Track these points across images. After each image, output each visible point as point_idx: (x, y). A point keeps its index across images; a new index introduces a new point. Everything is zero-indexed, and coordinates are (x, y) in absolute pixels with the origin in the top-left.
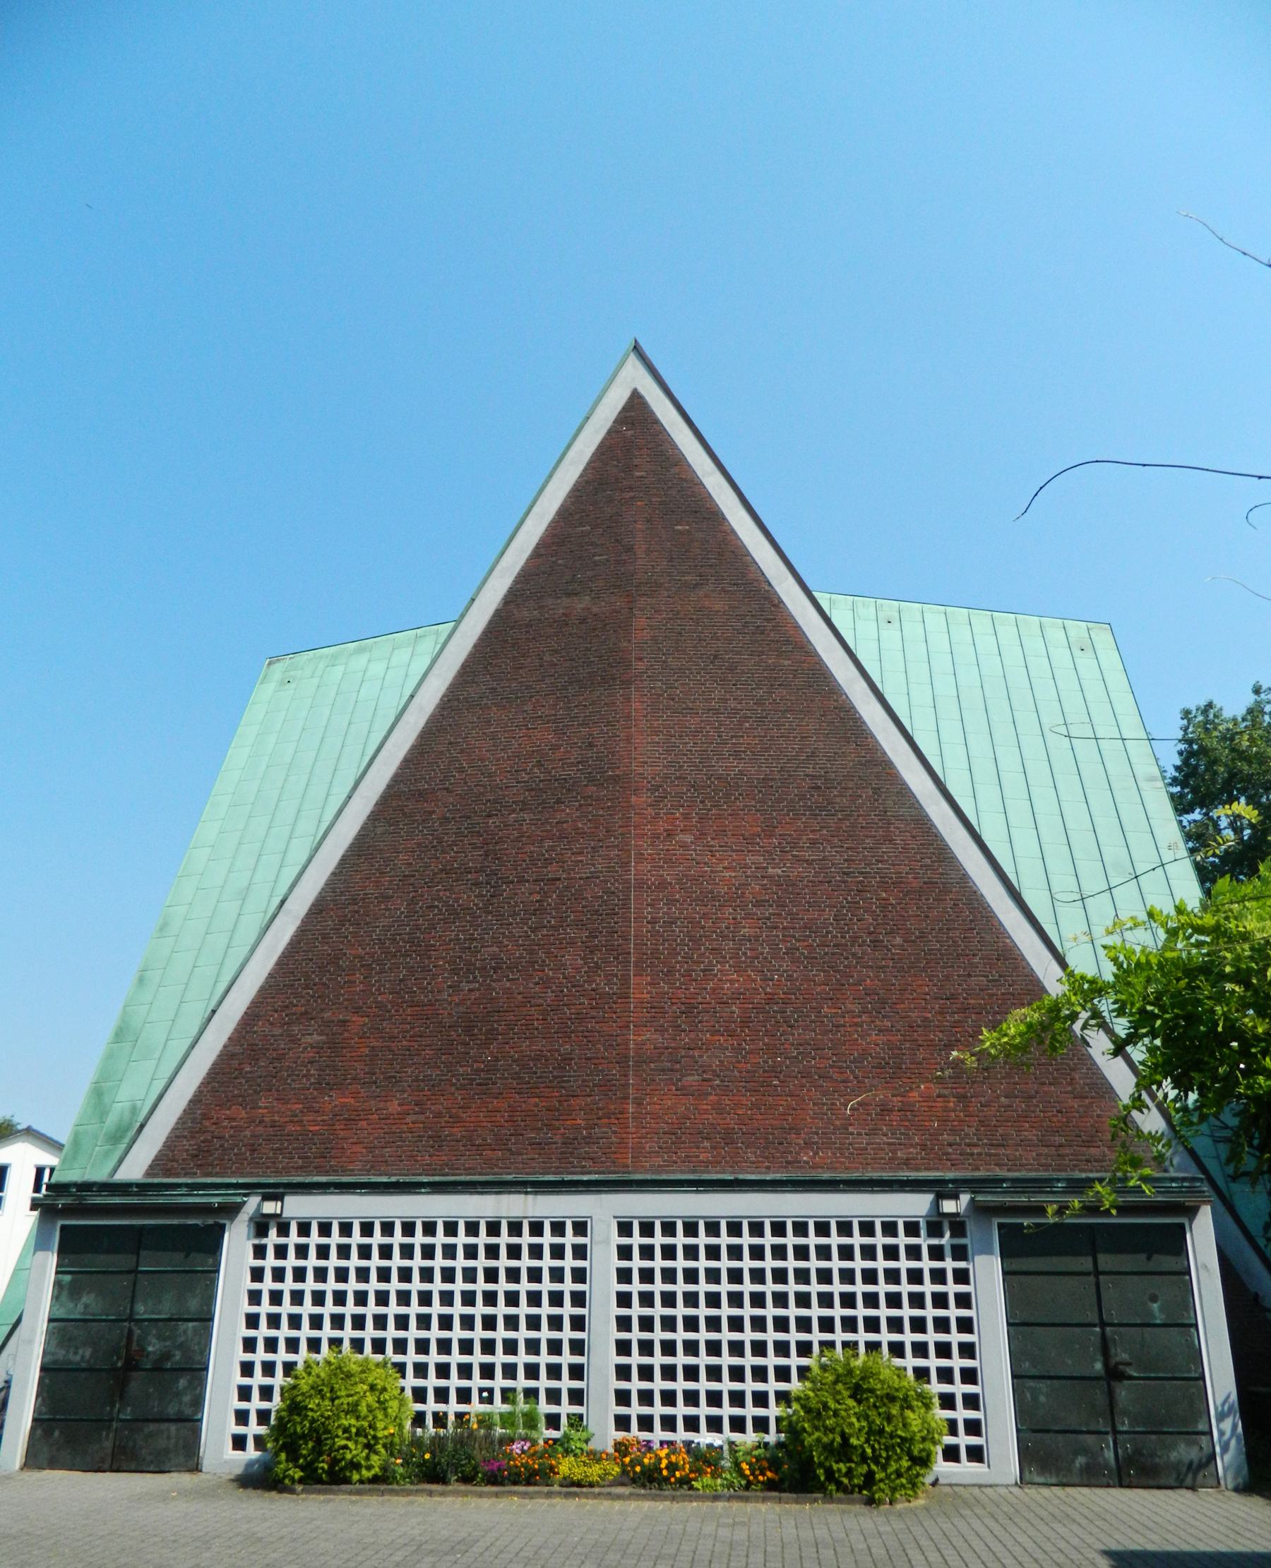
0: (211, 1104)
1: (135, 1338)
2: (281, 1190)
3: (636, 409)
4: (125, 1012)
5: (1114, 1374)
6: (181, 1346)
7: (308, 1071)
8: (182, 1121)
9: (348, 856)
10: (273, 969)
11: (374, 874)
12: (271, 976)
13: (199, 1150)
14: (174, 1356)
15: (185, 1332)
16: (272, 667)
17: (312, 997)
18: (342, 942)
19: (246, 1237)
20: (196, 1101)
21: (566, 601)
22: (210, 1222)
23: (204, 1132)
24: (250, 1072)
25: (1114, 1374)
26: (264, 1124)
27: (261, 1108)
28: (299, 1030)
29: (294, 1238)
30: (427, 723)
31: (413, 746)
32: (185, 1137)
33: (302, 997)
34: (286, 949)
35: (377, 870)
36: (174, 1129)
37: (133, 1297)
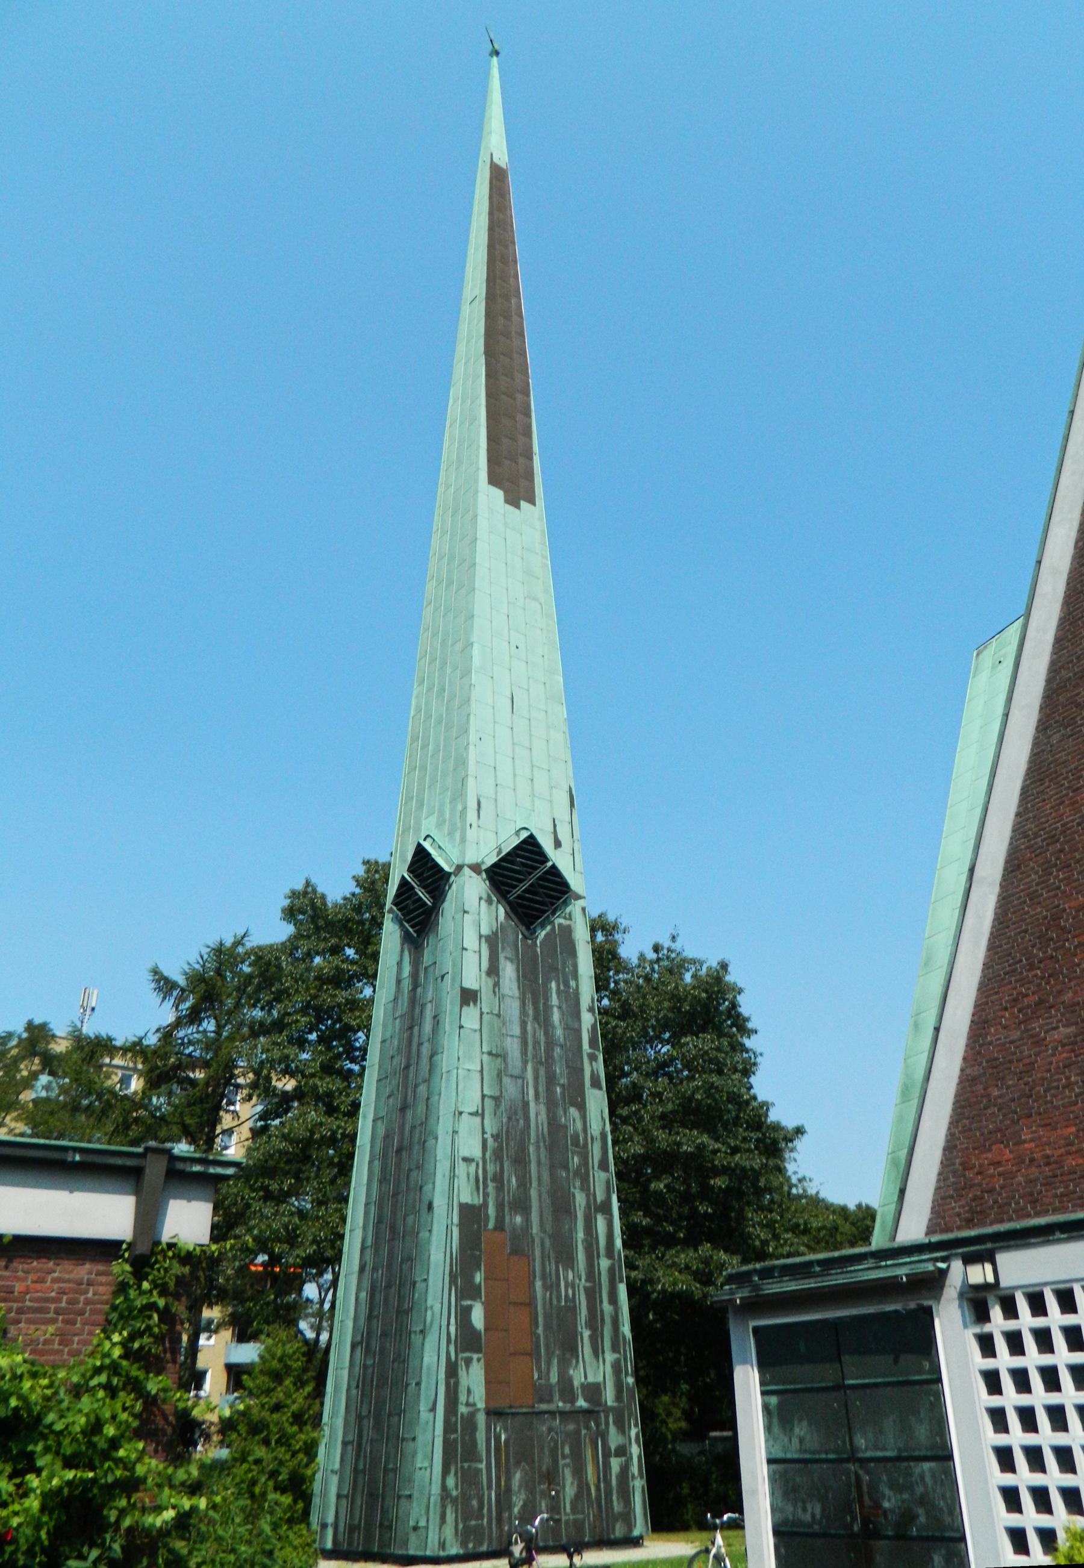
0: (967, 1148)
1: (865, 1489)
2: (989, 1245)
4: (907, 1067)
6: (923, 1501)
7: (1068, 1078)
8: (942, 1176)
9: (1028, 786)
10: (986, 957)
11: (1067, 795)
12: (987, 966)
13: (972, 1211)
14: (918, 1516)
15: (922, 1477)
16: (981, 656)
17: (1043, 978)
18: (1056, 896)
19: (962, 1327)
20: (950, 1148)
22: (912, 1305)
23: (971, 1186)
24: (1000, 1097)
26: (1036, 1163)
27: (1025, 1142)
28: (1041, 1027)
29: (1026, 1320)
30: (1068, 584)
31: (1060, 619)
32: (952, 1197)
33: (1030, 982)
34: (993, 927)
35: (1069, 788)
36: (938, 1189)
37: (850, 1429)
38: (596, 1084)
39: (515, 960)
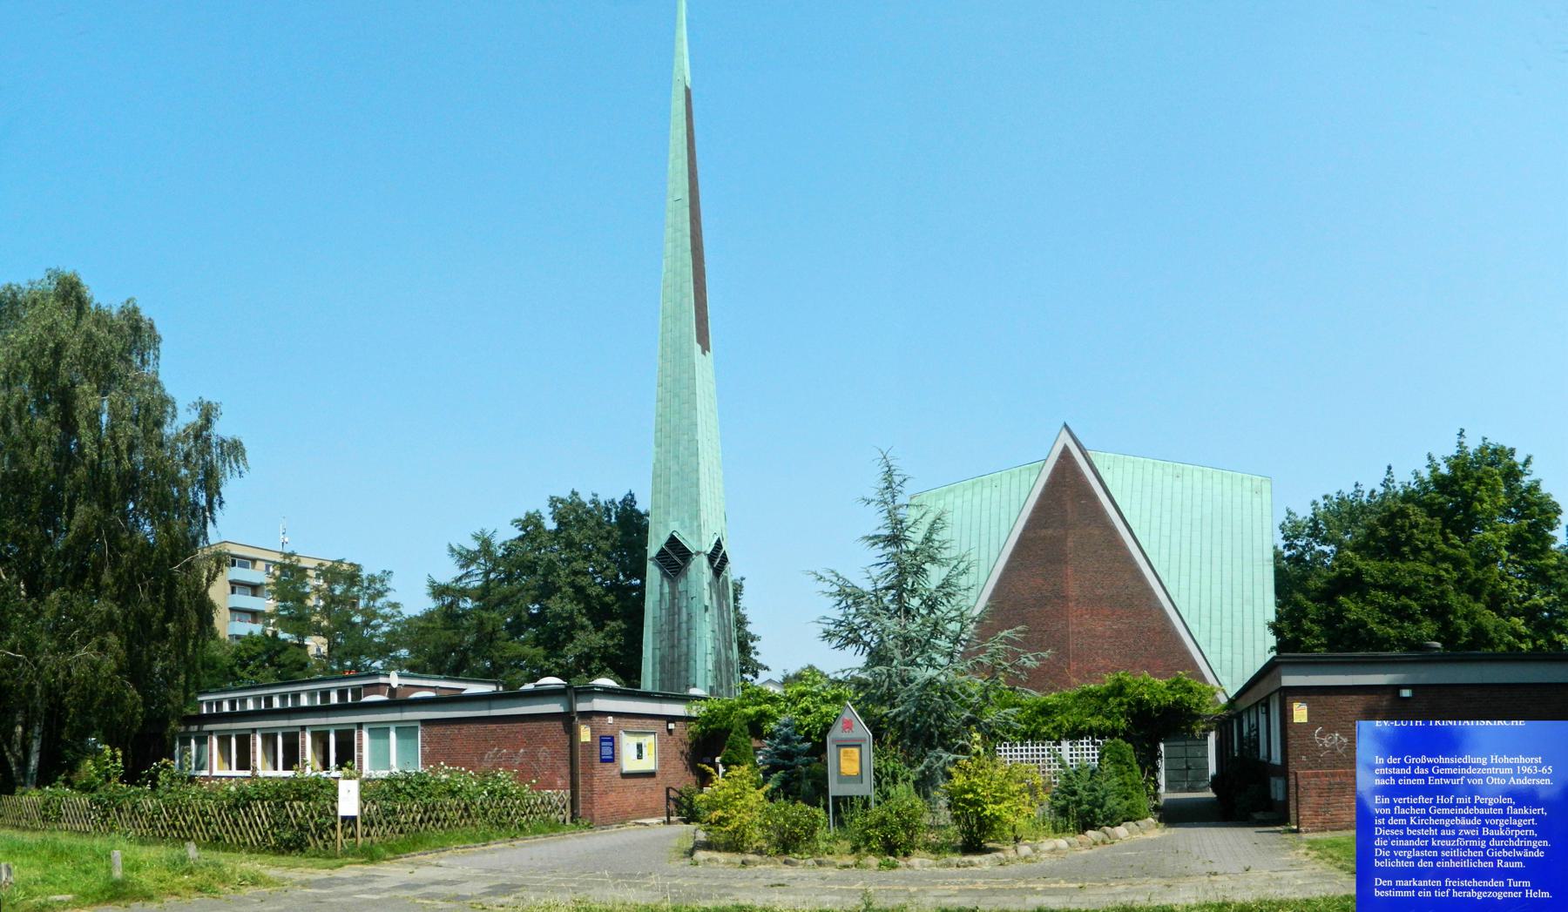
3: (1066, 453)
5: (1188, 768)
21: (1044, 530)
25: (1188, 768)
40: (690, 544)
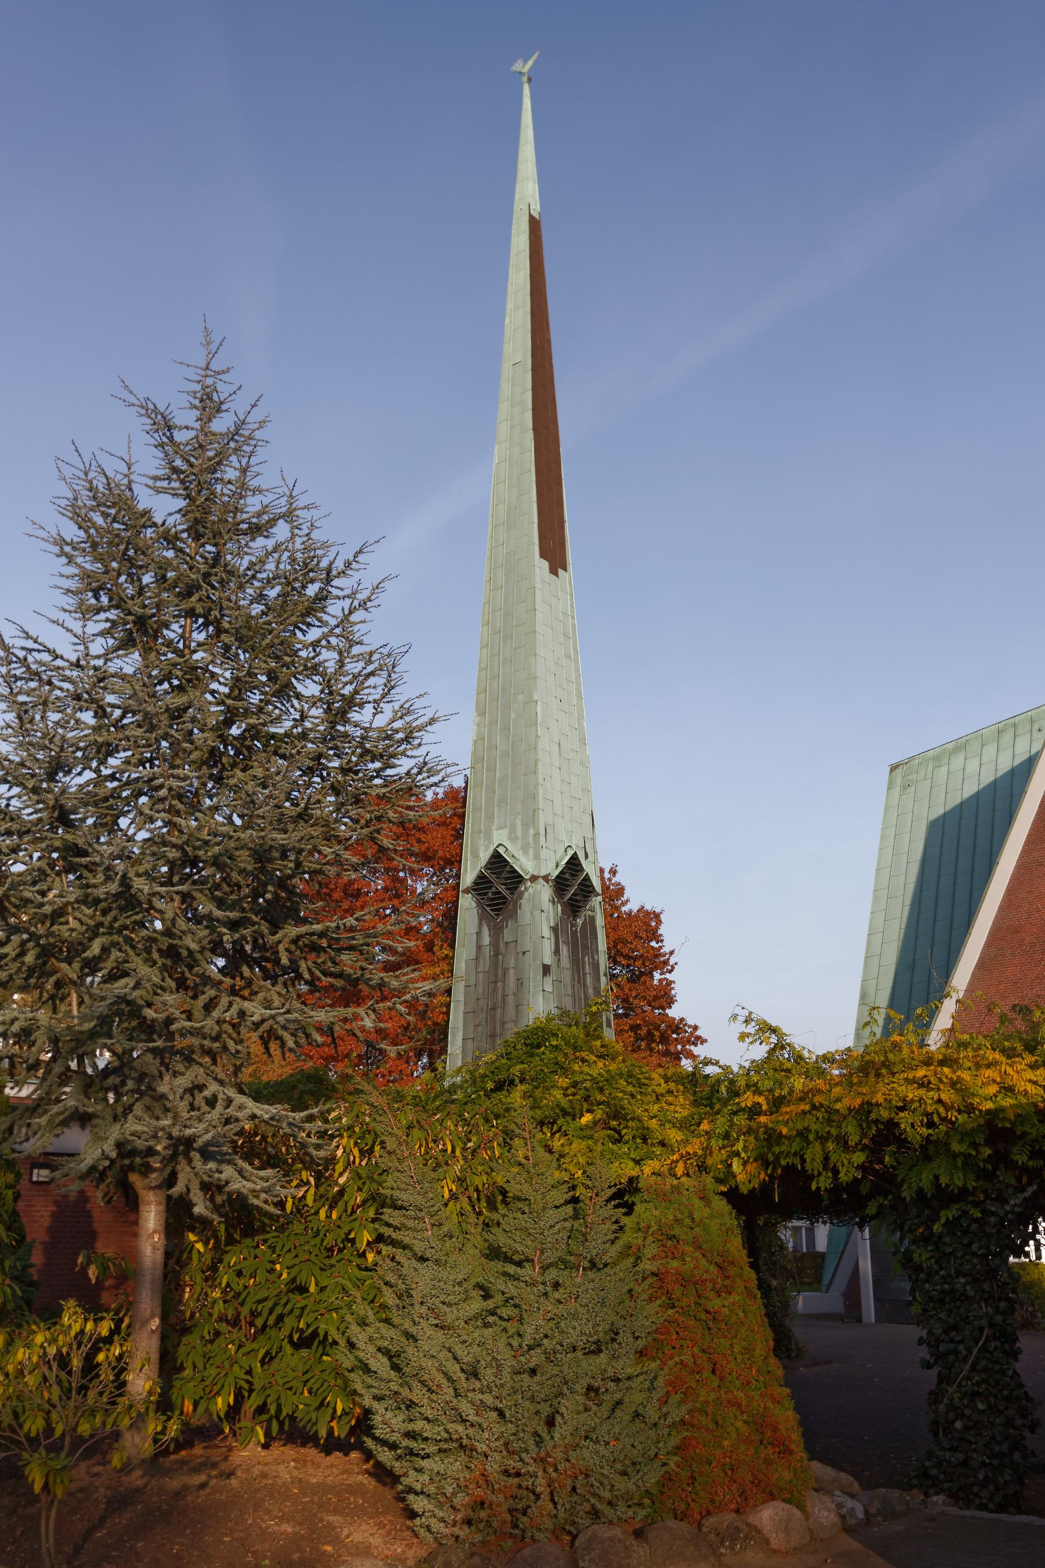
38: (609, 1025)
39: (566, 943)
40: (524, 863)
